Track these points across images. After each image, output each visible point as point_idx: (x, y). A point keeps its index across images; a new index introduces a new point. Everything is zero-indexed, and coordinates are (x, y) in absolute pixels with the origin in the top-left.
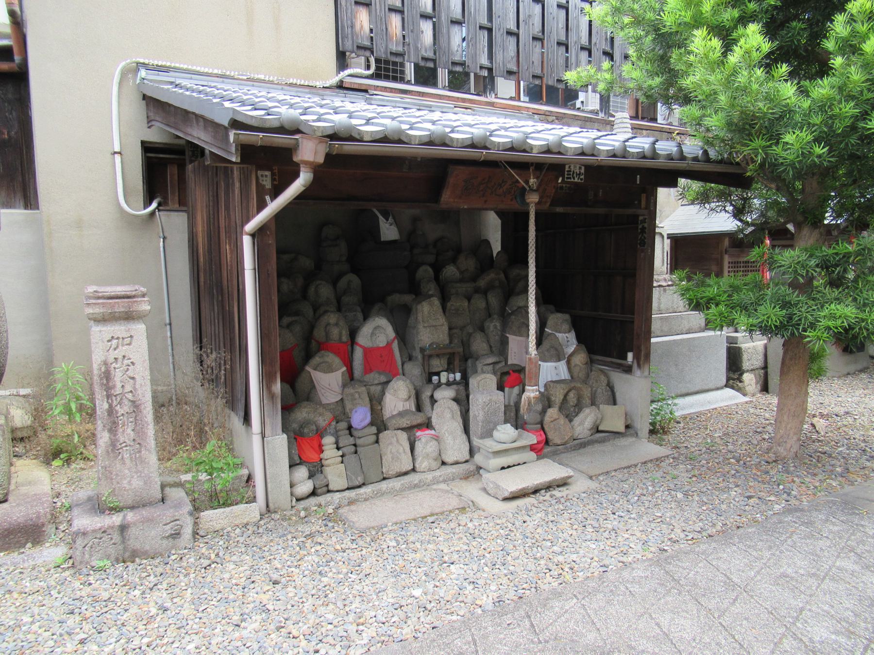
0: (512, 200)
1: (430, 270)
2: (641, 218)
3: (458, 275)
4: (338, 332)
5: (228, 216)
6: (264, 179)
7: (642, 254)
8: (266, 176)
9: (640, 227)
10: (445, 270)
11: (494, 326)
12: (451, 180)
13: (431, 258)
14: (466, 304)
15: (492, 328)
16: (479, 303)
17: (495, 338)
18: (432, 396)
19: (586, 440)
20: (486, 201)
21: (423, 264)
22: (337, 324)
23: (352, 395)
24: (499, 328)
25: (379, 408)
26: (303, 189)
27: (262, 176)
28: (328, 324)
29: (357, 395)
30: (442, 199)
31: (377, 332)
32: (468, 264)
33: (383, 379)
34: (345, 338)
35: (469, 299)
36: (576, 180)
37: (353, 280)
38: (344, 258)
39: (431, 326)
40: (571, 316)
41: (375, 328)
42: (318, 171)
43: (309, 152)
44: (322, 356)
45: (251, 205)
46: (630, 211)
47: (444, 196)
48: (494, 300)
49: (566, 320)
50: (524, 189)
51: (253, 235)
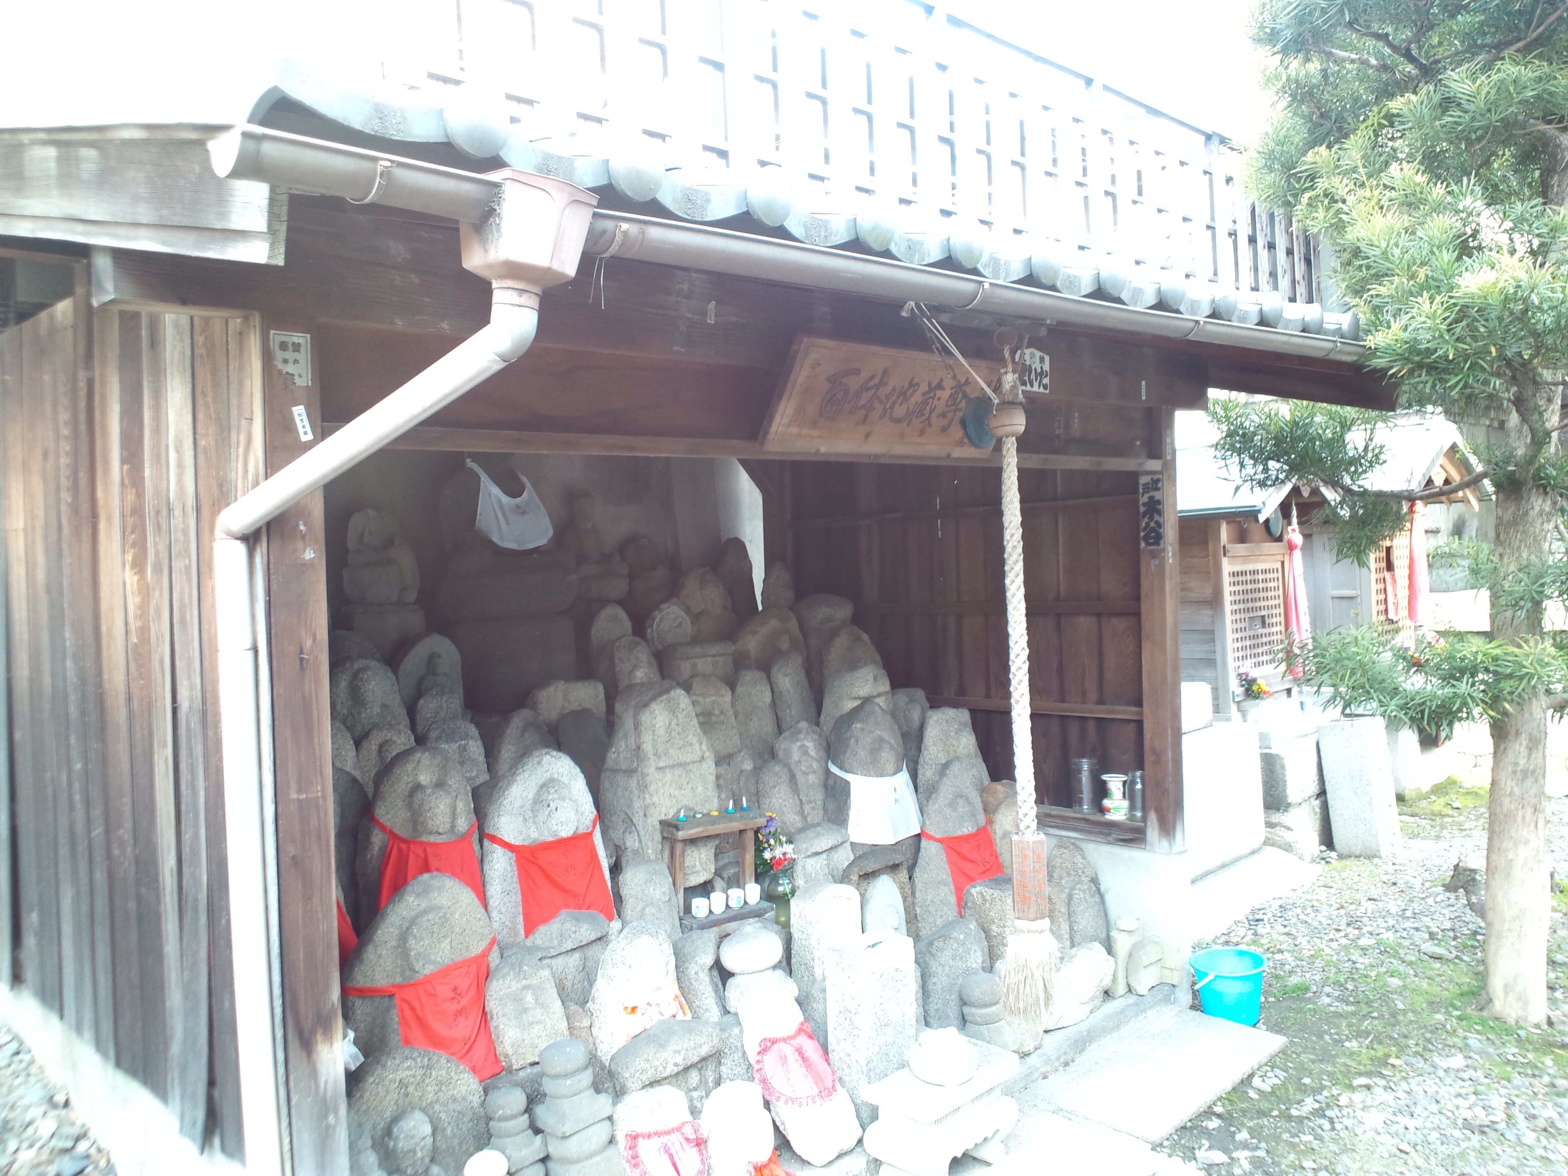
0: (922, 433)
1: (623, 616)
2: (1144, 480)
3: (688, 627)
4: (446, 814)
5: (134, 477)
6: (290, 355)
7: (1155, 562)
8: (297, 347)
9: (1144, 499)
10: (658, 615)
11: (803, 749)
12: (801, 376)
13: (619, 587)
14: (728, 698)
15: (796, 756)
16: (756, 691)
17: (811, 779)
18: (718, 965)
19: (1084, 1027)
20: (867, 436)
21: (604, 602)
22: (440, 785)
23: (517, 999)
24: (812, 753)
25: (586, 1023)
26: (498, 366)
27: (283, 346)
28: (417, 788)
29: (529, 998)
30: (774, 428)
31: (548, 797)
32: (709, 596)
33: (586, 933)
34: (463, 824)
35: (732, 685)
36: (1036, 388)
37: (442, 647)
38: (412, 596)
39: (676, 761)
40: (973, 712)
41: (545, 786)
42: (558, 301)
43: (536, 233)
44: (426, 891)
45: (238, 438)
46: (1129, 464)
47: (777, 420)
48: (789, 679)
49: (966, 725)
50: (983, 402)
51: (250, 539)
